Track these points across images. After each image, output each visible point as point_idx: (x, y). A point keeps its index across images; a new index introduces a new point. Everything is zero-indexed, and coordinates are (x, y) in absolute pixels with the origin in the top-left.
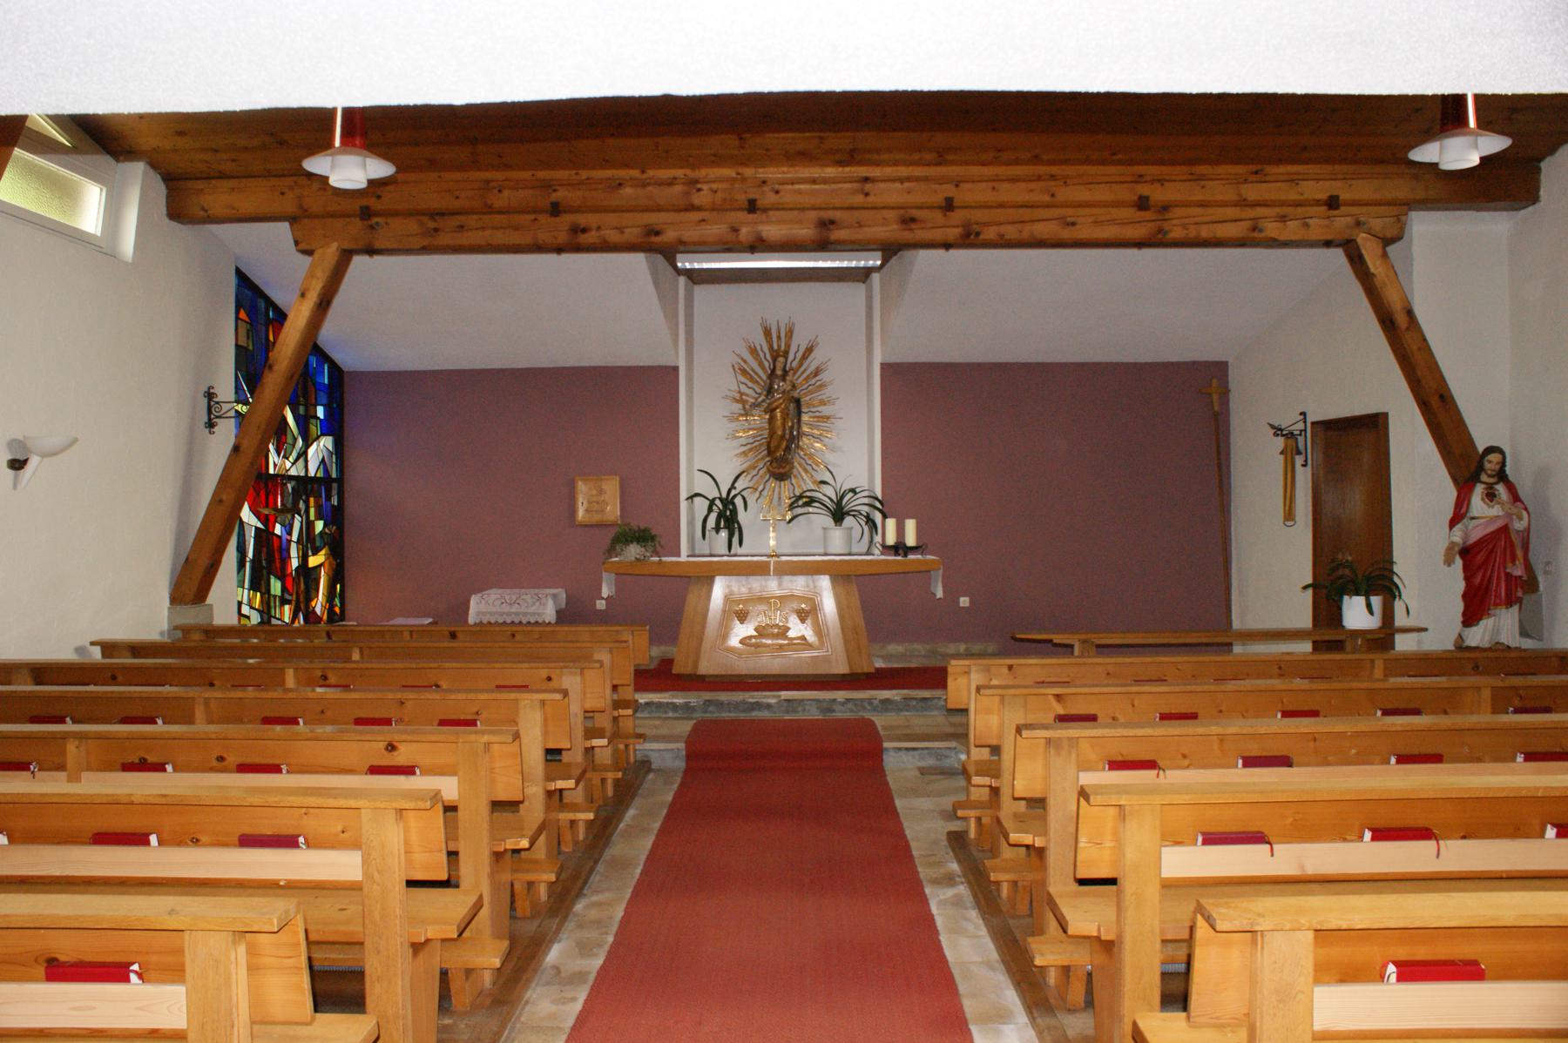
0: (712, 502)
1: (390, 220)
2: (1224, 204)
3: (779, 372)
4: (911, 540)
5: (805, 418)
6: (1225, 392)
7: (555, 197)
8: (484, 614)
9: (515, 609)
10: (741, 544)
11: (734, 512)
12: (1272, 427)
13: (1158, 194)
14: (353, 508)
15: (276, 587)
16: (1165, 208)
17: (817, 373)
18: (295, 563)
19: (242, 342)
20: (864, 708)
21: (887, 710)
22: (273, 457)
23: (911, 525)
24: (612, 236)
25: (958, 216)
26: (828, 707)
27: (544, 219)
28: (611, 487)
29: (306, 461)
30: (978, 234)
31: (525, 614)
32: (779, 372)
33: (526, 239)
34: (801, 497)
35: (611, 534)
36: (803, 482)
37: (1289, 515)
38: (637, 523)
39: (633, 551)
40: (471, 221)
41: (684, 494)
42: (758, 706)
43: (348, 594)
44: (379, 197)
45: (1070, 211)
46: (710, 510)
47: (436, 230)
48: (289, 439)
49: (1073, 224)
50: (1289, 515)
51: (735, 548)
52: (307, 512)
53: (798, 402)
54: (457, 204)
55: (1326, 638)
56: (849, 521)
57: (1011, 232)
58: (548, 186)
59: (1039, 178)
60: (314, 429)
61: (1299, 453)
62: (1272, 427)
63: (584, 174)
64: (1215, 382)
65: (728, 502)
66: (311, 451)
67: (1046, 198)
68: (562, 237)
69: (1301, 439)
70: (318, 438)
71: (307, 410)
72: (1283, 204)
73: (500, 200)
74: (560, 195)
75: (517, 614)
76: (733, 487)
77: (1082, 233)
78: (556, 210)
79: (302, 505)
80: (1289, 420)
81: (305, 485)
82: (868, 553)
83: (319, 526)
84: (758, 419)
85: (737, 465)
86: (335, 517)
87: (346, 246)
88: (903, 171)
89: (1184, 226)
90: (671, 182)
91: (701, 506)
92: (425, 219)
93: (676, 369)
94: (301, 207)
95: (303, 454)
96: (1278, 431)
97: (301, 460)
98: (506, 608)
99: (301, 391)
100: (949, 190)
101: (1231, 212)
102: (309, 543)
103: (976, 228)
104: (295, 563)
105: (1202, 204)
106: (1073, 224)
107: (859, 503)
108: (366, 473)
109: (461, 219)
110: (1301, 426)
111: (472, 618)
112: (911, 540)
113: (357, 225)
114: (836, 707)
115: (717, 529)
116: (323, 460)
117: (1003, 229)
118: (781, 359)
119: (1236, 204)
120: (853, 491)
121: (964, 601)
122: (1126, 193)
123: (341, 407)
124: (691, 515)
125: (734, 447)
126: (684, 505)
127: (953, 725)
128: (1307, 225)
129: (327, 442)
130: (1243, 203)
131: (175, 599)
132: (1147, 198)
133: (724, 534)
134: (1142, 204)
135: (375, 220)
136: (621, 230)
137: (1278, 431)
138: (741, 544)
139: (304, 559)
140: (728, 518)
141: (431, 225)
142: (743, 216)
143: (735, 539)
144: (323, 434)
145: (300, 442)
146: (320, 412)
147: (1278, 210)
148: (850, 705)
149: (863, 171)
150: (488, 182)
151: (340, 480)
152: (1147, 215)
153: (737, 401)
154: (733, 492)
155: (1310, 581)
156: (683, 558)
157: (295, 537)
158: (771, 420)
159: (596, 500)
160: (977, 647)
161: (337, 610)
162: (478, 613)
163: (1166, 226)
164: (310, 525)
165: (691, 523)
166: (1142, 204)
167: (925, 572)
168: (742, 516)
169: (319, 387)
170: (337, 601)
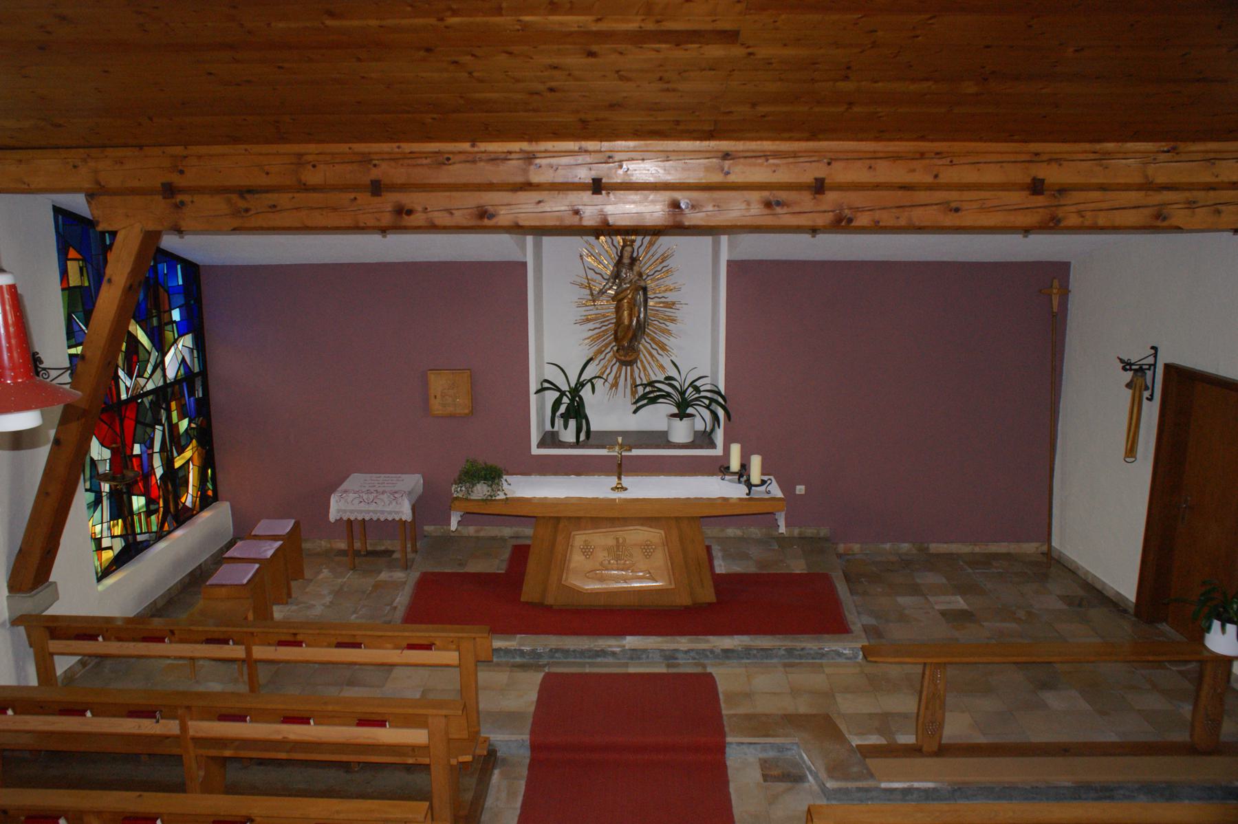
1: (196, 198)
2: (1127, 187)
3: (626, 261)
5: (651, 303)
6: (1065, 292)
7: (375, 174)
8: (345, 511)
9: (373, 507)
12: (1121, 361)
13: (1053, 175)
14: (218, 397)
15: (138, 502)
16: (1063, 190)
17: (664, 259)
18: (159, 472)
19: (74, 280)
20: (707, 657)
21: (728, 658)
22: (125, 381)
24: (441, 219)
25: (831, 197)
26: (670, 657)
27: (364, 198)
29: (164, 370)
30: (850, 220)
31: (383, 512)
32: (626, 261)
33: (348, 222)
36: (652, 369)
37: (1131, 451)
40: (283, 199)
41: (533, 387)
42: (603, 653)
43: (220, 477)
44: (182, 172)
45: (953, 195)
47: (247, 210)
48: (142, 355)
49: (957, 210)
50: (1131, 451)
52: (169, 418)
53: (645, 289)
54: (264, 181)
57: (886, 218)
58: (366, 160)
59: (922, 155)
60: (169, 335)
61: (1147, 388)
62: (1121, 361)
63: (407, 147)
64: (1056, 283)
65: (575, 391)
66: (168, 359)
67: (929, 179)
68: (387, 220)
69: (1149, 374)
70: (175, 341)
71: (159, 320)
72: (1190, 187)
73: (312, 177)
74: (384, 171)
75: (375, 512)
77: (967, 219)
78: (377, 188)
79: (163, 414)
80: (1138, 354)
81: (164, 394)
83: (184, 425)
84: (606, 306)
86: (202, 411)
87: (151, 227)
88: (768, 145)
89: (1080, 213)
90: (505, 157)
92: (234, 197)
93: (524, 264)
94: (98, 183)
95: (160, 364)
96: (1127, 365)
97: (159, 371)
98: (363, 507)
99: (147, 301)
100: (819, 171)
101: (1134, 197)
102: (175, 441)
103: (847, 212)
104: (159, 472)
105: (1102, 188)
106: (957, 210)
108: (228, 364)
109: (272, 198)
110: (1151, 360)
111: (333, 516)
113: (160, 205)
114: (680, 655)
116: (183, 359)
117: (877, 215)
118: (628, 249)
119: (1139, 187)
121: (800, 489)
122: (1019, 175)
123: (199, 300)
124: (539, 410)
125: (585, 331)
126: (533, 398)
127: (795, 692)
128: (1219, 212)
129: (187, 340)
130: (1148, 186)
131: (15, 586)
132: (1042, 181)
134: (1037, 187)
135: (179, 198)
136: (450, 212)
137: (1127, 365)
139: (168, 463)
141: (242, 204)
142: (587, 196)
144: (181, 335)
145: (155, 354)
146: (176, 315)
147: (1187, 194)
148: (692, 654)
149: (725, 145)
150: (300, 155)
151: (204, 373)
152: (1040, 200)
153: (582, 286)
157: (157, 448)
158: (618, 309)
161: (210, 493)
162: (339, 511)
163: (1060, 213)
164: (173, 428)
166: (1037, 187)
169: (170, 292)
170: (209, 485)
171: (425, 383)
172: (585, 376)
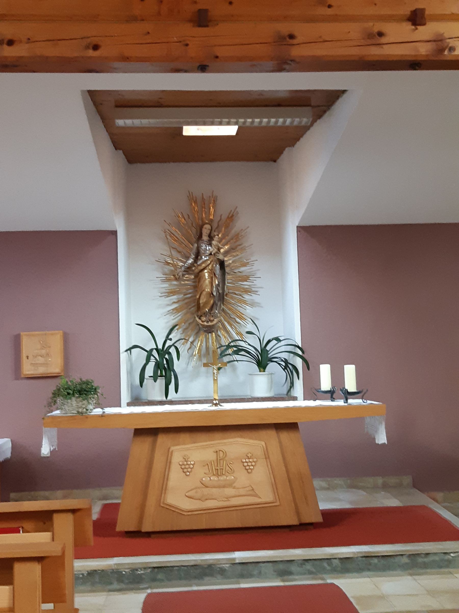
0: (150, 353)
3: (205, 238)
4: (351, 384)
10: (176, 391)
11: (170, 362)
23: (350, 371)
25: (426, 31)
26: (284, 568)
28: (56, 341)
34: (229, 347)
35: (52, 385)
38: (77, 377)
39: (73, 405)
41: (123, 346)
42: (207, 571)
46: (148, 360)
51: (172, 395)
55: (158, 560)
56: (272, 366)
76: (168, 338)
82: (289, 397)
85: (172, 320)
91: (139, 357)
93: (114, 233)
107: (278, 351)
112: (351, 384)
114: (294, 568)
115: (155, 378)
120: (278, 339)
126: (123, 356)
133: (161, 382)
138: (176, 391)
140: (164, 368)
142: (189, 31)
143: (172, 387)
148: (308, 566)
154: (169, 343)
155: (84, 380)
156: (125, 410)
159: (43, 354)
160: (393, 480)
165: (130, 373)
167: (356, 419)
168: (178, 366)
171: (17, 342)
172: (169, 343)
